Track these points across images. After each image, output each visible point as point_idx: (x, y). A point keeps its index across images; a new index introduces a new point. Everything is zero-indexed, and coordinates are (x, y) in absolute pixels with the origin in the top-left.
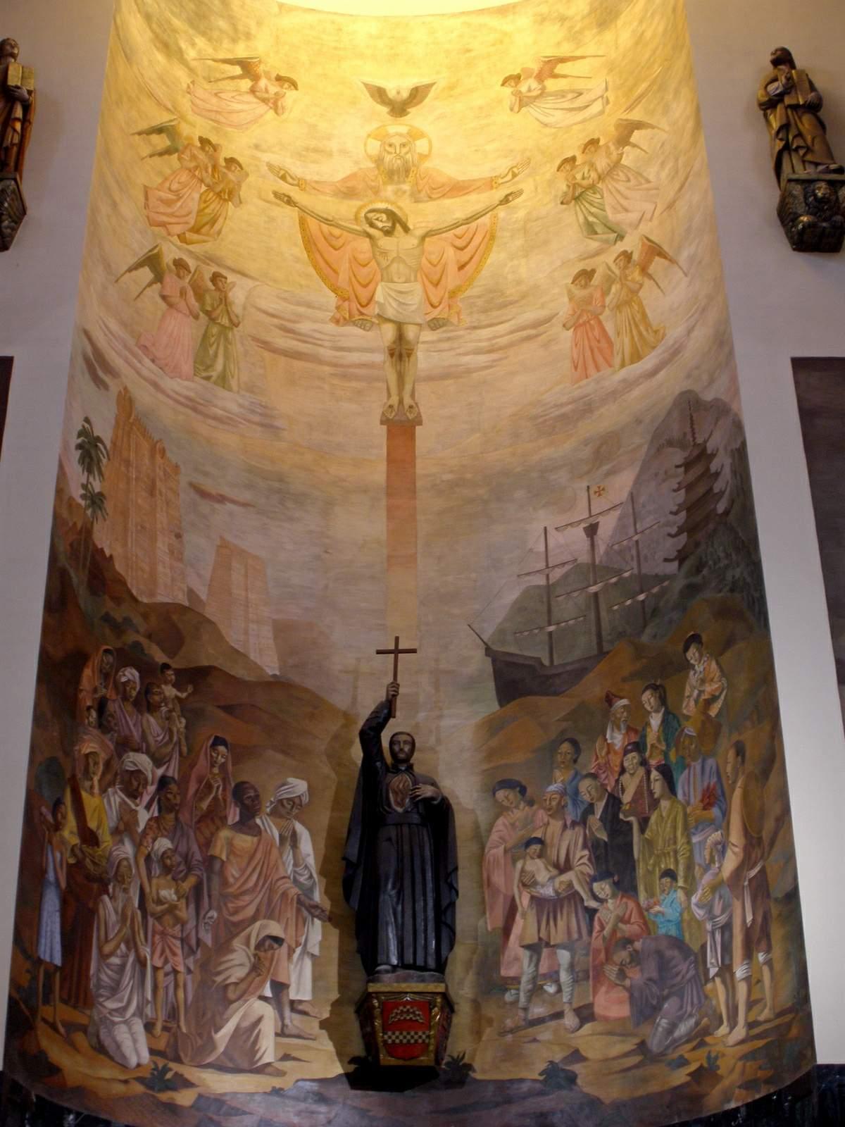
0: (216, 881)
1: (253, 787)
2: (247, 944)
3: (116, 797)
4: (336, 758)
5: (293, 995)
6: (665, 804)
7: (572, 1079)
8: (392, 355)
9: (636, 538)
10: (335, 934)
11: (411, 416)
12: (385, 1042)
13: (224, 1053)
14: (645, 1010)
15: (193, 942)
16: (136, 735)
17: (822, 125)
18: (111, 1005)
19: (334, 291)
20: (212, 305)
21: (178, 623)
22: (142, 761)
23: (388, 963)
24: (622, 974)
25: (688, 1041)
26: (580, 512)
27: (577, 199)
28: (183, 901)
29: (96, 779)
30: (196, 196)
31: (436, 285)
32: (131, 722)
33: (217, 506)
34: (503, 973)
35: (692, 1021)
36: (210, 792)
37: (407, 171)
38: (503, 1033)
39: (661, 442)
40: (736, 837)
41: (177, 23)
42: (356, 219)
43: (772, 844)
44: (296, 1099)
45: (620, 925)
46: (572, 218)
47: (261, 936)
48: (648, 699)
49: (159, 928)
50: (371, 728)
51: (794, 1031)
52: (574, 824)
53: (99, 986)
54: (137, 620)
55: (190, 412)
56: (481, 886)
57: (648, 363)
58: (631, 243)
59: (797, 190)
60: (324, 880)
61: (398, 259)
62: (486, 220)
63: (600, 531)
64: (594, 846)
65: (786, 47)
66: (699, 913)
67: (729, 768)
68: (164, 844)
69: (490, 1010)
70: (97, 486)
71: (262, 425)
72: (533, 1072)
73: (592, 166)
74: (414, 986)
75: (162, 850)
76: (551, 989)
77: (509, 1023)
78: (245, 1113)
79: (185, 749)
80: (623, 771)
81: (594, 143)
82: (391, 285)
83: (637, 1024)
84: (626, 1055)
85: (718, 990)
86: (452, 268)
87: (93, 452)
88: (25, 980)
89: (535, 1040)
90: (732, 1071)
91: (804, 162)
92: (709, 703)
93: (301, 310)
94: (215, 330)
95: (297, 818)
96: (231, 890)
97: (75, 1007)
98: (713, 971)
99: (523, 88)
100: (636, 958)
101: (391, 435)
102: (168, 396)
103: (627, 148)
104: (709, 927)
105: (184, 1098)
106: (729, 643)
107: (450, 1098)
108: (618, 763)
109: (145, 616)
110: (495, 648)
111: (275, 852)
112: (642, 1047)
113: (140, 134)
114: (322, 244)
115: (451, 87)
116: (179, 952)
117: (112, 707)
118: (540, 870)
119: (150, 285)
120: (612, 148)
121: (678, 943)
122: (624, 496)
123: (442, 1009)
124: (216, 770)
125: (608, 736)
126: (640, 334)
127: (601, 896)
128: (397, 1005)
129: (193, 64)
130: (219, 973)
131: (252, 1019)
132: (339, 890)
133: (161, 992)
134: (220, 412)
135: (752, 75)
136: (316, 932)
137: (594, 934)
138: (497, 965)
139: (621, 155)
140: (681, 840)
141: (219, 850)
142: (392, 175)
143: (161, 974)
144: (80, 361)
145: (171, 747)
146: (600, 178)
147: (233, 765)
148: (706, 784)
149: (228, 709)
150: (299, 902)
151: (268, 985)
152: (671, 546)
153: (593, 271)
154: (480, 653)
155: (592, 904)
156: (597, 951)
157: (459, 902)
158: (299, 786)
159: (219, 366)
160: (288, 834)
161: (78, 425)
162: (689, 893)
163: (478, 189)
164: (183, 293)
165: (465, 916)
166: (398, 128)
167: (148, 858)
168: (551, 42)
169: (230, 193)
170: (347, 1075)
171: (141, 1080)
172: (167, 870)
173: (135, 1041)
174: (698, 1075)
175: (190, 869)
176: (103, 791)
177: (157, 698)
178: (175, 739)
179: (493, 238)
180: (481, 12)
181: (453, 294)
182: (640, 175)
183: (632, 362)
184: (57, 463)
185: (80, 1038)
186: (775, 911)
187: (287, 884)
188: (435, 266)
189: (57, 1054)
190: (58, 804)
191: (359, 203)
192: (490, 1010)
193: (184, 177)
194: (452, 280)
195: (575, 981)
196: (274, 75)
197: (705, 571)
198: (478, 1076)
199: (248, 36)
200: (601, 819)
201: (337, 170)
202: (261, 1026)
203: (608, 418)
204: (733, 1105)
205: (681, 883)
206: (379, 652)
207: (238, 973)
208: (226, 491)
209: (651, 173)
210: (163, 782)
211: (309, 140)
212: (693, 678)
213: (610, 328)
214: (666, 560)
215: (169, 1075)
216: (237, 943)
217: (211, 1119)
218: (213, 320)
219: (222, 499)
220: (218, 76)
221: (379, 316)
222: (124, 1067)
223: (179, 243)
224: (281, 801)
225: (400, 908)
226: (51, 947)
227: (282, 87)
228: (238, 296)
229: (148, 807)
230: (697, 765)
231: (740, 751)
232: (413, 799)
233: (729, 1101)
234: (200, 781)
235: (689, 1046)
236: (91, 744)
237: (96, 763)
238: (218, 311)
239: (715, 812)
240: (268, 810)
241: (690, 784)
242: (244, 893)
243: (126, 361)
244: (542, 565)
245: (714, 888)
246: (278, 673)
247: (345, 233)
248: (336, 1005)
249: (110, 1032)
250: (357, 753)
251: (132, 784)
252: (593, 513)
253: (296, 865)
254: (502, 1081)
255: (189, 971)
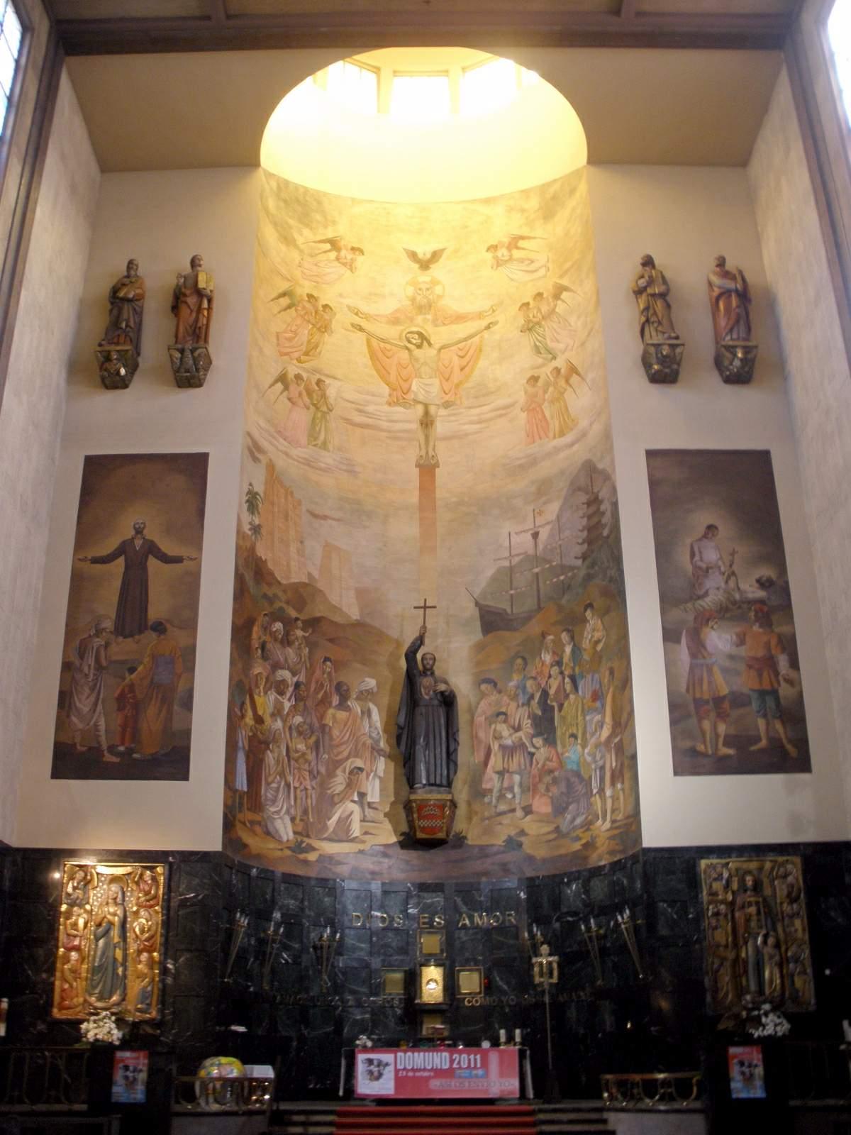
0: (327, 737)
1: (346, 684)
2: (344, 771)
3: (272, 695)
4: (392, 667)
5: (369, 799)
6: (572, 697)
7: (520, 845)
8: (422, 424)
9: (560, 542)
10: (392, 765)
11: (433, 462)
12: (420, 826)
13: (333, 831)
14: (559, 810)
15: (315, 772)
16: (282, 660)
17: (668, 306)
18: (272, 809)
19: (388, 385)
20: (317, 400)
21: (303, 594)
22: (284, 674)
23: (421, 783)
24: (548, 790)
25: (582, 827)
26: (529, 525)
27: (530, 330)
28: (309, 751)
29: (261, 688)
30: (306, 332)
31: (447, 380)
32: (278, 653)
33: (322, 522)
34: (484, 786)
35: (584, 816)
36: (322, 688)
37: (430, 306)
38: (483, 819)
39: (575, 488)
40: (608, 719)
41: (291, 222)
42: (400, 338)
43: (626, 727)
44: (372, 855)
45: (548, 763)
46: (527, 341)
47: (352, 767)
48: (565, 637)
49: (297, 765)
50: (411, 652)
51: (633, 828)
52: (523, 705)
53: (266, 800)
54: (280, 594)
55: (306, 467)
56: (472, 738)
57: (568, 438)
58: (560, 363)
59: (652, 350)
60: (386, 735)
61: (425, 363)
62: (476, 339)
63: (540, 536)
64: (533, 717)
65: (653, 257)
66: (589, 759)
67: (606, 680)
68: (298, 719)
69: (476, 807)
70: (257, 522)
71: (345, 471)
72: (499, 840)
73: (539, 310)
74: (436, 796)
75: (297, 723)
76: (509, 796)
77: (486, 814)
78: (344, 864)
79: (308, 665)
80: (550, 676)
81: (540, 295)
82: (421, 380)
83: (555, 817)
84: (549, 833)
85: (597, 800)
86: (457, 370)
87: (254, 502)
88: (230, 802)
89: (500, 824)
90: (603, 844)
91: (657, 331)
92: (597, 642)
93: (369, 398)
94: (319, 415)
95: (370, 700)
96: (334, 743)
97: (254, 812)
98: (595, 791)
99: (499, 254)
100: (555, 781)
101: (421, 475)
102: (294, 460)
103: (559, 302)
104: (593, 766)
105: (312, 857)
106: (607, 611)
107: (454, 854)
108: (548, 671)
109: (285, 591)
110: (482, 602)
111: (359, 720)
112: (557, 829)
113: (272, 300)
114: (380, 355)
115: (456, 251)
116: (308, 778)
117: (269, 646)
118: (504, 730)
119: (281, 393)
120: (551, 300)
121: (577, 774)
122: (554, 517)
123: (450, 808)
124: (325, 676)
125: (542, 656)
126: (564, 419)
127: (537, 745)
128: (426, 806)
129: (302, 247)
130: (329, 789)
131: (347, 813)
132: (394, 741)
133: (299, 801)
134: (323, 465)
135: (629, 271)
136: (382, 765)
137: (533, 766)
138: (480, 781)
139: (555, 306)
140: (580, 718)
141: (328, 721)
142: (422, 308)
143: (298, 791)
144: (246, 452)
145: (300, 665)
146: (543, 318)
147: (335, 672)
148: (594, 688)
149: (331, 640)
150: (373, 748)
151: (356, 794)
152: (579, 550)
153: (539, 377)
154: (472, 605)
155: (533, 750)
156: (534, 777)
157: (460, 748)
158: (371, 683)
159: (322, 437)
160: (365, 710)
161: (246, 488)
162: (584, 747)
163: (472, 319)
164: (300, 394)
165: (463, 756)
166: (424, 278)
167: (290, 728)
168: (516, 225)
169: (326, 327)
170: (400, 842)
171: (289, 848)
172: (300, 733)
173: (285, 828)
174: (586, 846)
175: (313, 732)
176: (266, 693)
177: (293, 638)
178: (303, 660)
179: (481, 350)
180: (474, 201)
181: (457, 386)
182: (567, 321)
183: (560, 436)
184: (236, 516)
185: (257, 829)
186: (626, 764)
187: (365, 738)
188: (446, 368)
189: (247, 838)
190: (243, 704)
191: (402, 328)
192: (476, 807)
193: (299, 321)
194: (455, 379)
195: (523, 792)
196: (349, 247)
197: (596, 568)
198: (470, 842)
199: (334, 223)
200: (538, 703)
201: (387, 307)
202: (352, 816)
203: (545, 469)
204: (602, 863)
205: (579, 741)
206: (415, 608)
207: (339, 788)
208: (327, 513)
209: (572, 320)
210: (297, 685)
211: (370, 290)
212: (589, 627)
213: (547, 414)
214: (576, 558)
215: (304, 845)
216: (339, 772)
217: (325, 867)
218: (317, 408)
219: (325, 517)
220: (317, 252)
221: (414, 400)
222: (280, 841)
223: (298, 364)
224: (361, 692)
225: (427, 752)
226: (242, 783)
227: (354, 253)
228: (331, 392)
229: (289, 700)
230: (589, 677)
231: (612, 672)
232: (434, 691)
233: (601, 860)
234: (317, 682)
235: (582, 830)
236: (259, 669)
237: (261, 678)
238: (321, 403)
239: (598, 704)
240: (355, 696)
241: (586, 687)
242: (342, 744)
243: (270, 442)
244: (507, 554)
245: (597, 746)
246: (359, 618)
247: (394, 348)
248: (393, 804)
249: (273, 823)
250: (403, 664)
251: (280, 688)
252: (537, 525)
253: (370, 727)
254: (483, 846)
255: (313, 788)
